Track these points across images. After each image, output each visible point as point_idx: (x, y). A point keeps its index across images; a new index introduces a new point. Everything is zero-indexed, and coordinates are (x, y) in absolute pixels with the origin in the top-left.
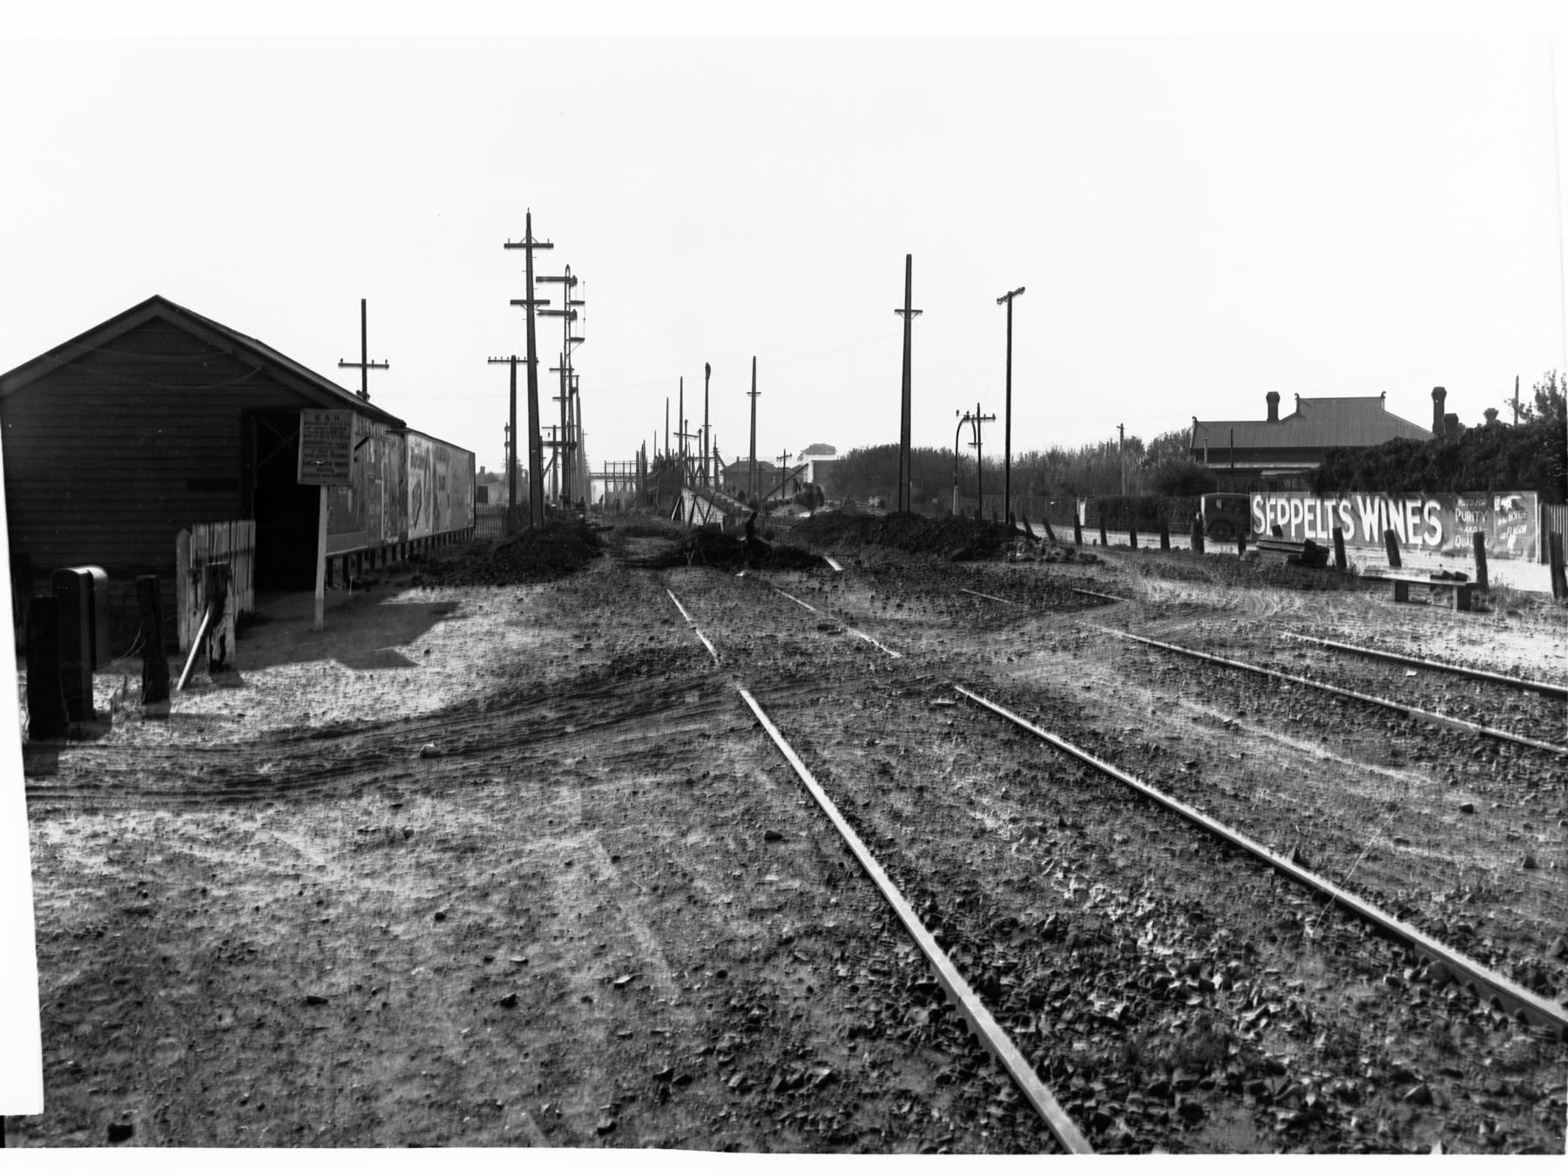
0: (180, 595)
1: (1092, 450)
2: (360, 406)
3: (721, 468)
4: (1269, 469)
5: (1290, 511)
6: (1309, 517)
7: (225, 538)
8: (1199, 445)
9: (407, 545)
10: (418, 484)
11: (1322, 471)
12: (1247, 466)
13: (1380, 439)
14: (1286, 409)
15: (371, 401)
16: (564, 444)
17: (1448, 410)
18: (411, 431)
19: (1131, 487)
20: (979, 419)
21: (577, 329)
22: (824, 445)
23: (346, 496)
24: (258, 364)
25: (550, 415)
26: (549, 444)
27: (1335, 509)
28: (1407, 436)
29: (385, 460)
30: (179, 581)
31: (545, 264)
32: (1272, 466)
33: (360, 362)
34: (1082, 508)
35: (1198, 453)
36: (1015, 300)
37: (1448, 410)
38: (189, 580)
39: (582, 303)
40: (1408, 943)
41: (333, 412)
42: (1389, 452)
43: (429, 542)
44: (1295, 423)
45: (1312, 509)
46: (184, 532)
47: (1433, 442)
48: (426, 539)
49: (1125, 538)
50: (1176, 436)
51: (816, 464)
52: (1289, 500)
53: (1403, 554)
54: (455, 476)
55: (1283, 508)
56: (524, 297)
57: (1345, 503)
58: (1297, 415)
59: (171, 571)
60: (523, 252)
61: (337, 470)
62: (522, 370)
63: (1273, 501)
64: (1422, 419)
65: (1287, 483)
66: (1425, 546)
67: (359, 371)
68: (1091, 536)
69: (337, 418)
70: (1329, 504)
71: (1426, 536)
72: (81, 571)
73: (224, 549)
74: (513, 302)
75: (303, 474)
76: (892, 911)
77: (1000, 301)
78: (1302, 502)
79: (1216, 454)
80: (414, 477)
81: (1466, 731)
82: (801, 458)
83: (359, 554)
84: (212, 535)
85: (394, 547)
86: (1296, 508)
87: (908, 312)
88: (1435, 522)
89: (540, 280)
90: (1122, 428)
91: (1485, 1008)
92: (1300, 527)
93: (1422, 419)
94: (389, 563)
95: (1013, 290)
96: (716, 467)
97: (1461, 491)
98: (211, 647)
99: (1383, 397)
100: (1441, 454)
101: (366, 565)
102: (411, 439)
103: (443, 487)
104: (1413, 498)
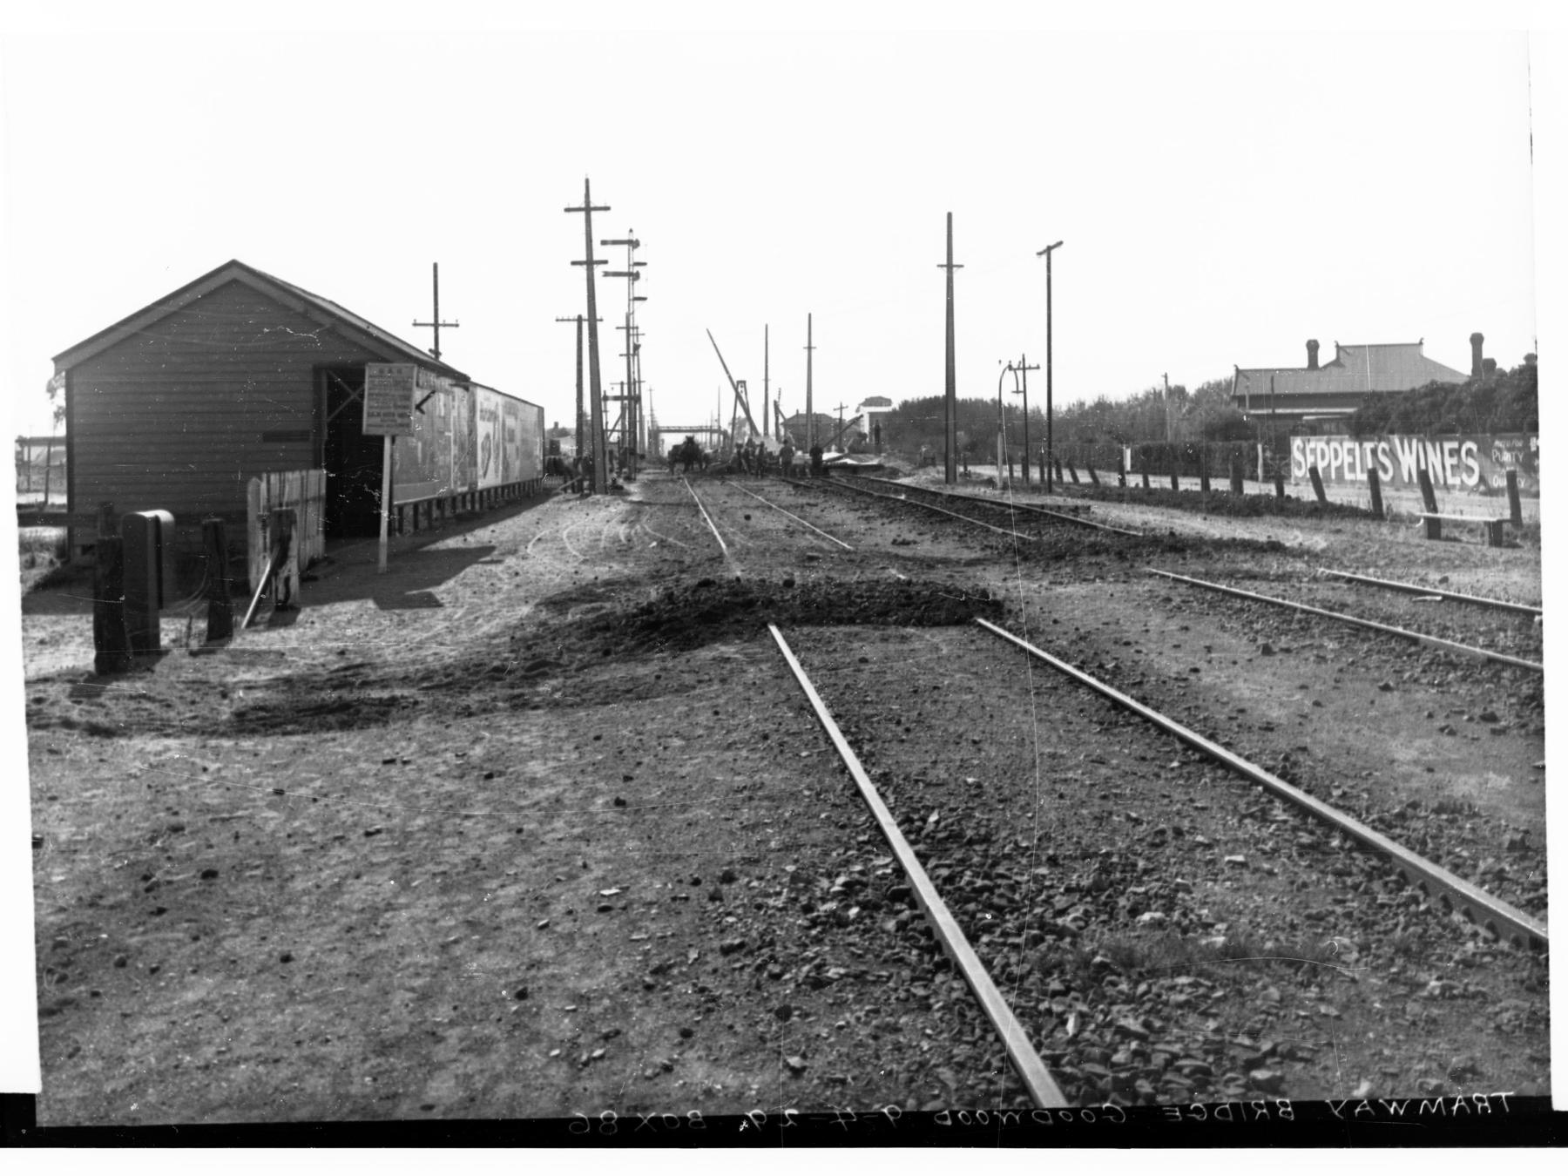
0: (251, 541)
1: (1136, 399)
2: (434, 366)
3: (781, 420)
4: (1310, 413)
5: (1329, 454)
6: (1348, 459)
7: (297, 485)
8: (1238, 394)
9: (477, 495)
10: (488, 437)
11: (1359, 416)
12: (1288, 411)
13: (1419, 382)
14: (1326, 356)
15: (442, 359)
16: (630, 398)
17: (1486, 355)
18: (476, 385)
19: (1177, 434)
20: (1024, 369)
21: (640, 288)
22: (881, 398)
23: (416, 448)
24: (327, 322)
25: (613, 376)
26: (616, 398)
27: (1374, 452)
28: (1442, 379)
29: (454, 413)
30: (250, 525)
31: (604, 226)
32: (1313, 411)
33: (432, 321)
34: (1128, 453)
35: (1240, 400)
36: (1053, 252)
37: (1486, 355)
38: (259, 525)
39: (644, 264)
40: (1385, 856)
41: (396, 365)
42: (1426, 395)
43: (500, 491)
44: (1335, 371)
45: (1351, 452)
46: (254, 479)
47: (1469, 384)
48: (496, 488)
49: (1166, 482)
50: (1218, 384)
51: (872, 415)
52: (1328, 443)
53: (1438, 494)
54: (524, 430)
55: (1323, 451)
56: (584, 258)
57: (1383, 445)
58: (1337, 363)
59: (243, 516)
60: (582, 215)
61: (399, 421)
62: (585, 325)
63: (1312, 445)
64: (1463, 366)
65: (1326, 427)
66: (1463, 487)
67: (432, 329)
68: (1134, 481)
69: (400, 371)
70: (1368, 446)
71: (1464, 477)
72: (149, 514)
73: (296, 496)
74: (574, 263)
75: (369, 425)
76: (879, 828)
77: (1040, 254)
78: (1341, 444)
79: (1257, 400)
80: (483, 428)
81: (1474, 657)
82: (858, 411)
83: (430, 502)
84: (282, 483)
85: (464, 495)
86: (1336, 451)
87: (950, 266)
88: (1471, 462)
89: (604, 243)
90: (1166, 377)
91: (1457, 917)
92: (1339, 469)
93: (1463, 366)
94: (459, 510)
95: (1052, 244)
96: (777, 419)
97: (1496, 431)
98: (277, 589)
99: (1421, 343)
100: (1475, 396)
101: (435, 513)
102: (480, 394)
103: (512, 440)
104: (1451, 439)
